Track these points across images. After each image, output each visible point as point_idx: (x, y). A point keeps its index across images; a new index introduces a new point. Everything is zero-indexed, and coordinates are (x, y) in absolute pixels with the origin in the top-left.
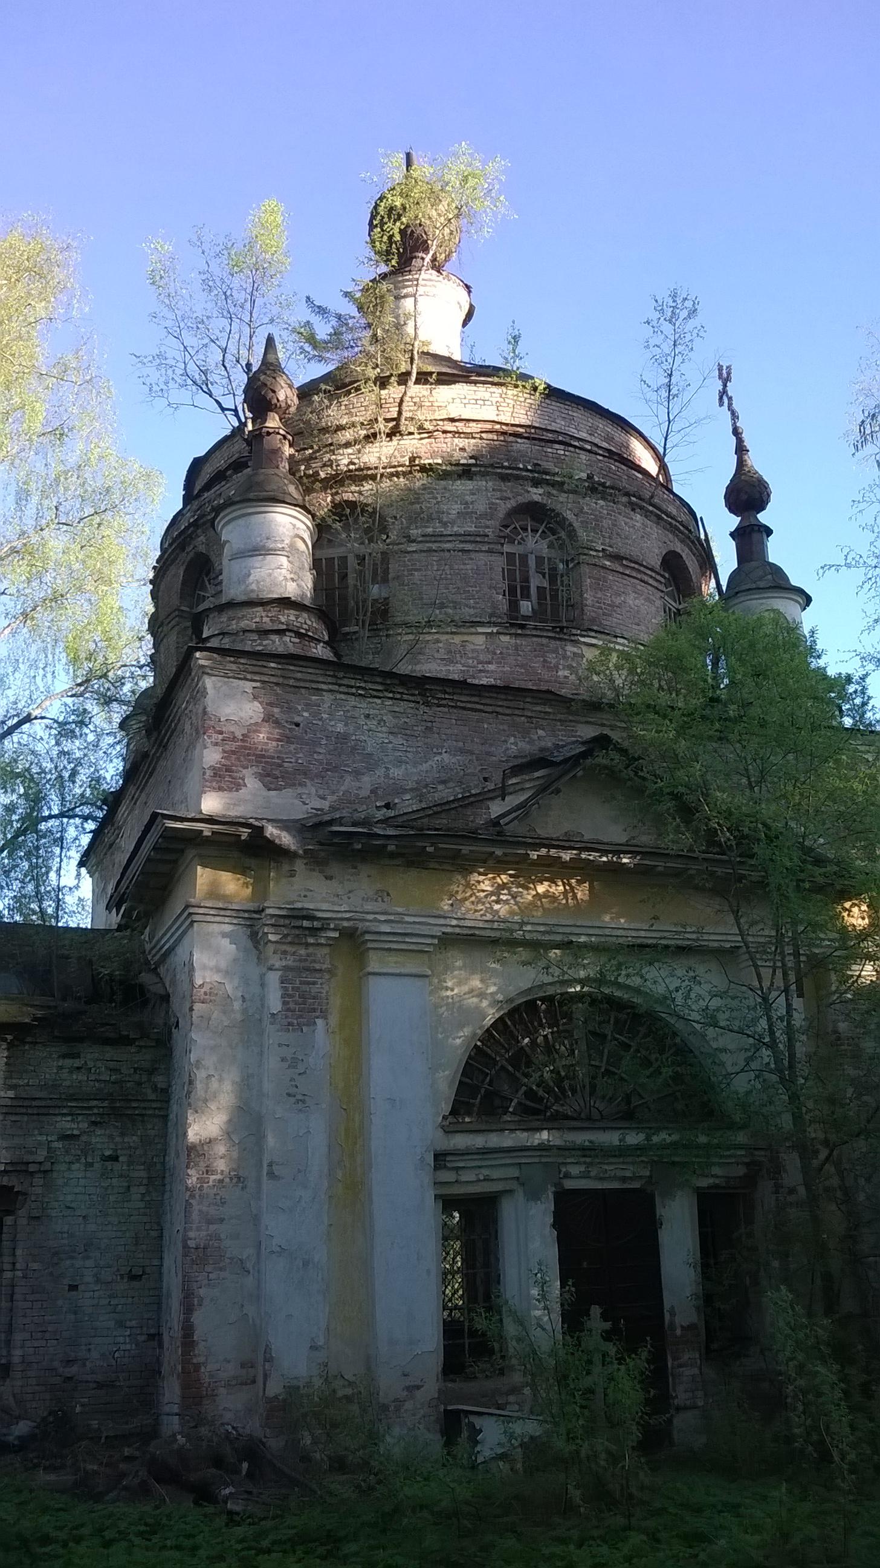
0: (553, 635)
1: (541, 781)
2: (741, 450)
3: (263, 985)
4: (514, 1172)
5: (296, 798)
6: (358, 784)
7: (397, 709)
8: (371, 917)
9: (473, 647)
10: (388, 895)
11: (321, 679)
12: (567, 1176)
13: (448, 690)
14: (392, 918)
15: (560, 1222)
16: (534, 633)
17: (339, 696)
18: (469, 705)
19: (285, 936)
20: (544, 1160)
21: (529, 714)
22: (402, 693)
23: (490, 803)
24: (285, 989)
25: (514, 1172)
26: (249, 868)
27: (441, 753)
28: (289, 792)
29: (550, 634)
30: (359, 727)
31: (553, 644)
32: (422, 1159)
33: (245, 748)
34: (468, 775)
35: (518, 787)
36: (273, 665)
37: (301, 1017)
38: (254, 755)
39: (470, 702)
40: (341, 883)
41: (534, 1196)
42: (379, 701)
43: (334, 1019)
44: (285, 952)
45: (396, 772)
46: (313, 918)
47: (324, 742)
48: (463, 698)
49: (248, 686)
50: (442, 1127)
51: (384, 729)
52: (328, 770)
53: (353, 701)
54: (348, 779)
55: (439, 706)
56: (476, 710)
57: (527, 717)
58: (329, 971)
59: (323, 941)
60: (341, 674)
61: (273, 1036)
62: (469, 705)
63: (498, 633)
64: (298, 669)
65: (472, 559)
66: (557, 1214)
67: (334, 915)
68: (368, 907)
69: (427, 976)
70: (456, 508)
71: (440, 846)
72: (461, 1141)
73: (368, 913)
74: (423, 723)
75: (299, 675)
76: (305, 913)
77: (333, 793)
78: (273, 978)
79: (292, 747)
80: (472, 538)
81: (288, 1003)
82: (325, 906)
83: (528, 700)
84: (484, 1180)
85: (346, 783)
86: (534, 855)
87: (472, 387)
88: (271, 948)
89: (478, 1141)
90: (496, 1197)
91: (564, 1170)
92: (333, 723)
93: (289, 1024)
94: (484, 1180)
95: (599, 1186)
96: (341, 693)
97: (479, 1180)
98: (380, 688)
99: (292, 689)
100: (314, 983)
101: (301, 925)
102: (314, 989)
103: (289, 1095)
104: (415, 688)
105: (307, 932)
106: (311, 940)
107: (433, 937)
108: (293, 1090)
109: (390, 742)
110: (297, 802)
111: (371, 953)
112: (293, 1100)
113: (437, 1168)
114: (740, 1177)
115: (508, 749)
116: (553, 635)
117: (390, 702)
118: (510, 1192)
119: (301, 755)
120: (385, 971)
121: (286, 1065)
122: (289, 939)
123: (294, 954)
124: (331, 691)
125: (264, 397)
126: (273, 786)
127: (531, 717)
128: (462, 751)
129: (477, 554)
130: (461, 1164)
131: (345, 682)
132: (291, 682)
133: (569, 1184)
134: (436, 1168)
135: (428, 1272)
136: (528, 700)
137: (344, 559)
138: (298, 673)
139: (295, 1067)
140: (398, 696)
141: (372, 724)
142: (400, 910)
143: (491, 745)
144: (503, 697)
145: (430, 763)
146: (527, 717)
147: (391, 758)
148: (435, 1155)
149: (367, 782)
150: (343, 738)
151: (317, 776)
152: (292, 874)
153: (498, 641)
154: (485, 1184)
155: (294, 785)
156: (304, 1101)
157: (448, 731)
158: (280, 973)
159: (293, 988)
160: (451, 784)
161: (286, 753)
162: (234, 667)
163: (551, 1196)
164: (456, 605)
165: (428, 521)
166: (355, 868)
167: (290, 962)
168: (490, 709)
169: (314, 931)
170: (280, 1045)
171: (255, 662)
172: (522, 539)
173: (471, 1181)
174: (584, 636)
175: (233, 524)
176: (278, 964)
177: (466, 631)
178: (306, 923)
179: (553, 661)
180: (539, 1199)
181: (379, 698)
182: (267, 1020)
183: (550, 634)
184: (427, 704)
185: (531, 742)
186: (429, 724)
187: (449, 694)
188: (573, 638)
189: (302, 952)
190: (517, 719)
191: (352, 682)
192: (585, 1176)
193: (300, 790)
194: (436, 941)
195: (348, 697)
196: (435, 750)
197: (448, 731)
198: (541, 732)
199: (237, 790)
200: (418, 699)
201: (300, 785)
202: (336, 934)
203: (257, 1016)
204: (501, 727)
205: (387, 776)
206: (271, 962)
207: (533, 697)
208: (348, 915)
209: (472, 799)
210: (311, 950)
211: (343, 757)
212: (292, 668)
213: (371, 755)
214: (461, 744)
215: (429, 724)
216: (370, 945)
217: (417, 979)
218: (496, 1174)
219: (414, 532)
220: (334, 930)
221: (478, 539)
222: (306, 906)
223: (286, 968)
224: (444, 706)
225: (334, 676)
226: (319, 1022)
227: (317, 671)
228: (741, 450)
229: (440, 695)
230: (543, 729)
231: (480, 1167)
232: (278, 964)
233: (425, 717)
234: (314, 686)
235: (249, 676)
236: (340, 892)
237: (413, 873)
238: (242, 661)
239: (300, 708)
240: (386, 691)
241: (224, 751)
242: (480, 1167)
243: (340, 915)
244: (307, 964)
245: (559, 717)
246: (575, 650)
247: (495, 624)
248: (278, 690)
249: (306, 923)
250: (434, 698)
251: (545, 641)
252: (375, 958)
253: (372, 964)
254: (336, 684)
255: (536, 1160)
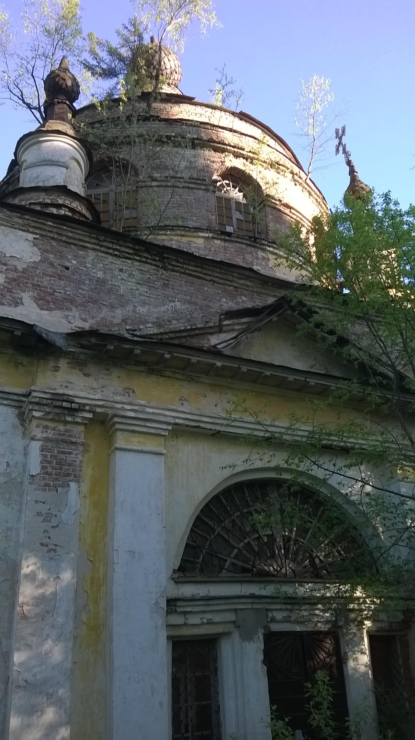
0: (249, 243)
1: (244, 327)
2: (352, 172)
3: (26, 455)
4: (231, 617)
5: (64, 318)
6: (112, 314)
7: (144, 269)
8: (119, 406)
9: (195, 245)
10: (134, 392)
11: (87, 239)
12: (273, 620)
13: (180, 260)
14: (136, 408)
15: (269, 659)
16: (237, 240)
17: (100, 254)
18: (194, 273)
19: (48, 413)
20: (255, 606)
21: (236, 285)
22: (146, 258)
23: (210, 337)
24: (45, 456)
25: (231, 617)
26: (21, 364)
27: (174, 301)
28: (58, 313)
29: (247, 242)
30: (114, 276)
31: (249, 249)
32: (157, 603)
33: (24, 278)
34: (193, 318)
35: (230, 328)
36: (50, 223)
37: (56, 479)
38: (31, 283)
39: (195, 271)
40: (96, 379)
41: (247, 637)
42: (130, 261)
43: (85, 487)
44: (46, 427)
45: (142, 310)
46: (72, 402)
47: (87, 282)
48: (190, 268)
49: (31, 237)
50: (173, 579)
51: (133, 280)
52: (89, 302)
53: (110, 259)
54: (105, 310)
55: (173, 271)
56: (199, 278)
57: (235, 287)
58: (83, 444)
59: (79, 420)
60: (102, 238)
61: (32, 494)
62: (194, 273)
63: (213, 238)
64: (70, 229)
65: (194, 193)
66: (266, 652)
67: (89, 402)
68: (118, 398)
69: (162, 454)
70: (183, 164)
71: (175, 354)
72: (188, 590)
73: (117, 403)
74: (161, 280)
75: (70, 234)
76: (65, 398)
77: (93, 318)
78: (35, 446)
79: (62, 283)
80: (195, 181)
81: (46, 468)
82: (82, 394)
83: (235, 275)
84: (208, 623)
85: (103, 312)
86: (244, 369)
87: (193, 107)
88: (35, 423)
89: (202, 590)
90: (216, 639)
91: (270, 615)
92: (95, 271)
93: (46, 485)
94: (208, 623)
95: (298, 629)
96: (101, 252)
97: (203, 624)
98: (131, 251)
99: (64, 244)
100: (70, 453)
101: (62, 407)
102: (70, 458)
103: (42, 544)
104: (156, 255)
105: (66, 412)
106: (69, 419)
107: (168, 424)
108: (45, 541)
109: (138, 289)
110: (64, 321)
111: (119, 433)
112: (45, 549)
113: (169, 612)
114: (399, 623)
115: (221, 305)
116: (249, 243)
117: (138, 264)
118: (228, 634)
119: (68, 289)
120: (129, 447)
121: (41, 519)
122: (50, 417)
123: (54, 429)
124: (94, 249)
125: (57, 83)
126: (45, 307)
127: (237, 287)
128: (190, 303)
129: (198, 191)
130: (189, 609)
131: (105, 244)
132: (64, 238)
133: (275, 627)
134: (168, 613)
135: (161, 704)
136: (235, 275)
137: (107, 194)
138: (68, 231)
139: (49, 521)
140: (144, 260)
141: (125, 276)
142: (143, 402)
143: (209, 301)
144: (219, 270)
145: (166, 306)
146: (235, 287)
147: (137, 300)
148: (167, 600)
149: (119, 314)
150: (102, 282)
151: (80, 305)
152: (57, 369)
153: (212, 243)
154: (207, 627)
155: (63, 309)
156: (55, 551)
157: (180, 288)
158: (40, 443)
159: (51, 456)
160: (182, 321)
161: (57, 286)
162: (20, 221)
163: (261, 637)
164: (183, 218)
165: (165, 170)
166: (109, 370)
167: (50, 434)
168: (209, 278)
169: (72, 411)
170: (36, 502)
171: (36, 219)
172: (227, 190)
173: (197, 624)
174: (269, 247)
175: (30, 149)
176: (39, 436)
177: (191, 234)
178: (65, 404)
179: (250, 260)
180: (252, 639)
181: (130, 259)
182: (26, 481)
183: (247, 242)
184: (165, 268)
185: (237, 303)
186: (166, 282)
187: (180, 263)
188: (262, 246)
189: (61, 428)
190: (228, 288)
191: (111, 245)
192: (287, 620)
193: (66, 313)
194: (170, 428)
195: (107, 256)
196: (170, 299)
197: (180, 288)
198: (244, 298)
199: (15, 306)
200: (159, 264)
201: (67, 309)
202: (90, 415)
203: (19, 480)
204: (217, 291)
205: (134, 311)
206: (33, 434)
207: (238, 274)
208: (101, 403)
209: (197, 332)
210: (69, 427)
211: (102, 294)
212: (65, 228)
213: (122, 296)
214: (189, 298)
215: (166, 282)
216: (117, 426)
217: (154, 456)
218: (217, 618)
219: (156, 175)
220: (90, 411)
221: (199, 182)
222: (67, 392)
223: (47, 440)
224: (177, 271)
225: (97, 239)
226: (73, 485)
227: (84, 233)
228: (352, 172)
229: (174, 263)
230: (246, 297)
231: (204, 612)
232: (39, 436)
233: (163, 276)
234: (81, 243)
235: (31, 230)
236: (95, 385)
237: (153, 379)
238: (26, 217)
239: (69, 257)
240: (136, 255)
241: (7, 278)
242: (204, 612)
243: (94, 402)
244: (65, 438)
245: (256, 290)
246: (264, 255)
247: (211, 231)
248: (54, 243)
249: (65, 404)
250: (169, 264)
251: (244, 246)
252: (121, 437)
253: (119, 442)
254: (98, 245)
255: (249, 606)
